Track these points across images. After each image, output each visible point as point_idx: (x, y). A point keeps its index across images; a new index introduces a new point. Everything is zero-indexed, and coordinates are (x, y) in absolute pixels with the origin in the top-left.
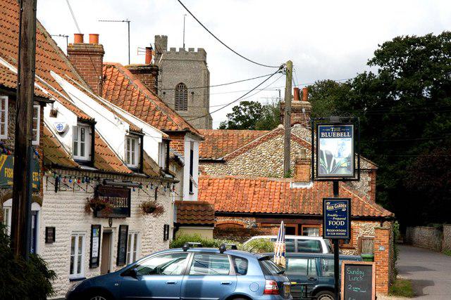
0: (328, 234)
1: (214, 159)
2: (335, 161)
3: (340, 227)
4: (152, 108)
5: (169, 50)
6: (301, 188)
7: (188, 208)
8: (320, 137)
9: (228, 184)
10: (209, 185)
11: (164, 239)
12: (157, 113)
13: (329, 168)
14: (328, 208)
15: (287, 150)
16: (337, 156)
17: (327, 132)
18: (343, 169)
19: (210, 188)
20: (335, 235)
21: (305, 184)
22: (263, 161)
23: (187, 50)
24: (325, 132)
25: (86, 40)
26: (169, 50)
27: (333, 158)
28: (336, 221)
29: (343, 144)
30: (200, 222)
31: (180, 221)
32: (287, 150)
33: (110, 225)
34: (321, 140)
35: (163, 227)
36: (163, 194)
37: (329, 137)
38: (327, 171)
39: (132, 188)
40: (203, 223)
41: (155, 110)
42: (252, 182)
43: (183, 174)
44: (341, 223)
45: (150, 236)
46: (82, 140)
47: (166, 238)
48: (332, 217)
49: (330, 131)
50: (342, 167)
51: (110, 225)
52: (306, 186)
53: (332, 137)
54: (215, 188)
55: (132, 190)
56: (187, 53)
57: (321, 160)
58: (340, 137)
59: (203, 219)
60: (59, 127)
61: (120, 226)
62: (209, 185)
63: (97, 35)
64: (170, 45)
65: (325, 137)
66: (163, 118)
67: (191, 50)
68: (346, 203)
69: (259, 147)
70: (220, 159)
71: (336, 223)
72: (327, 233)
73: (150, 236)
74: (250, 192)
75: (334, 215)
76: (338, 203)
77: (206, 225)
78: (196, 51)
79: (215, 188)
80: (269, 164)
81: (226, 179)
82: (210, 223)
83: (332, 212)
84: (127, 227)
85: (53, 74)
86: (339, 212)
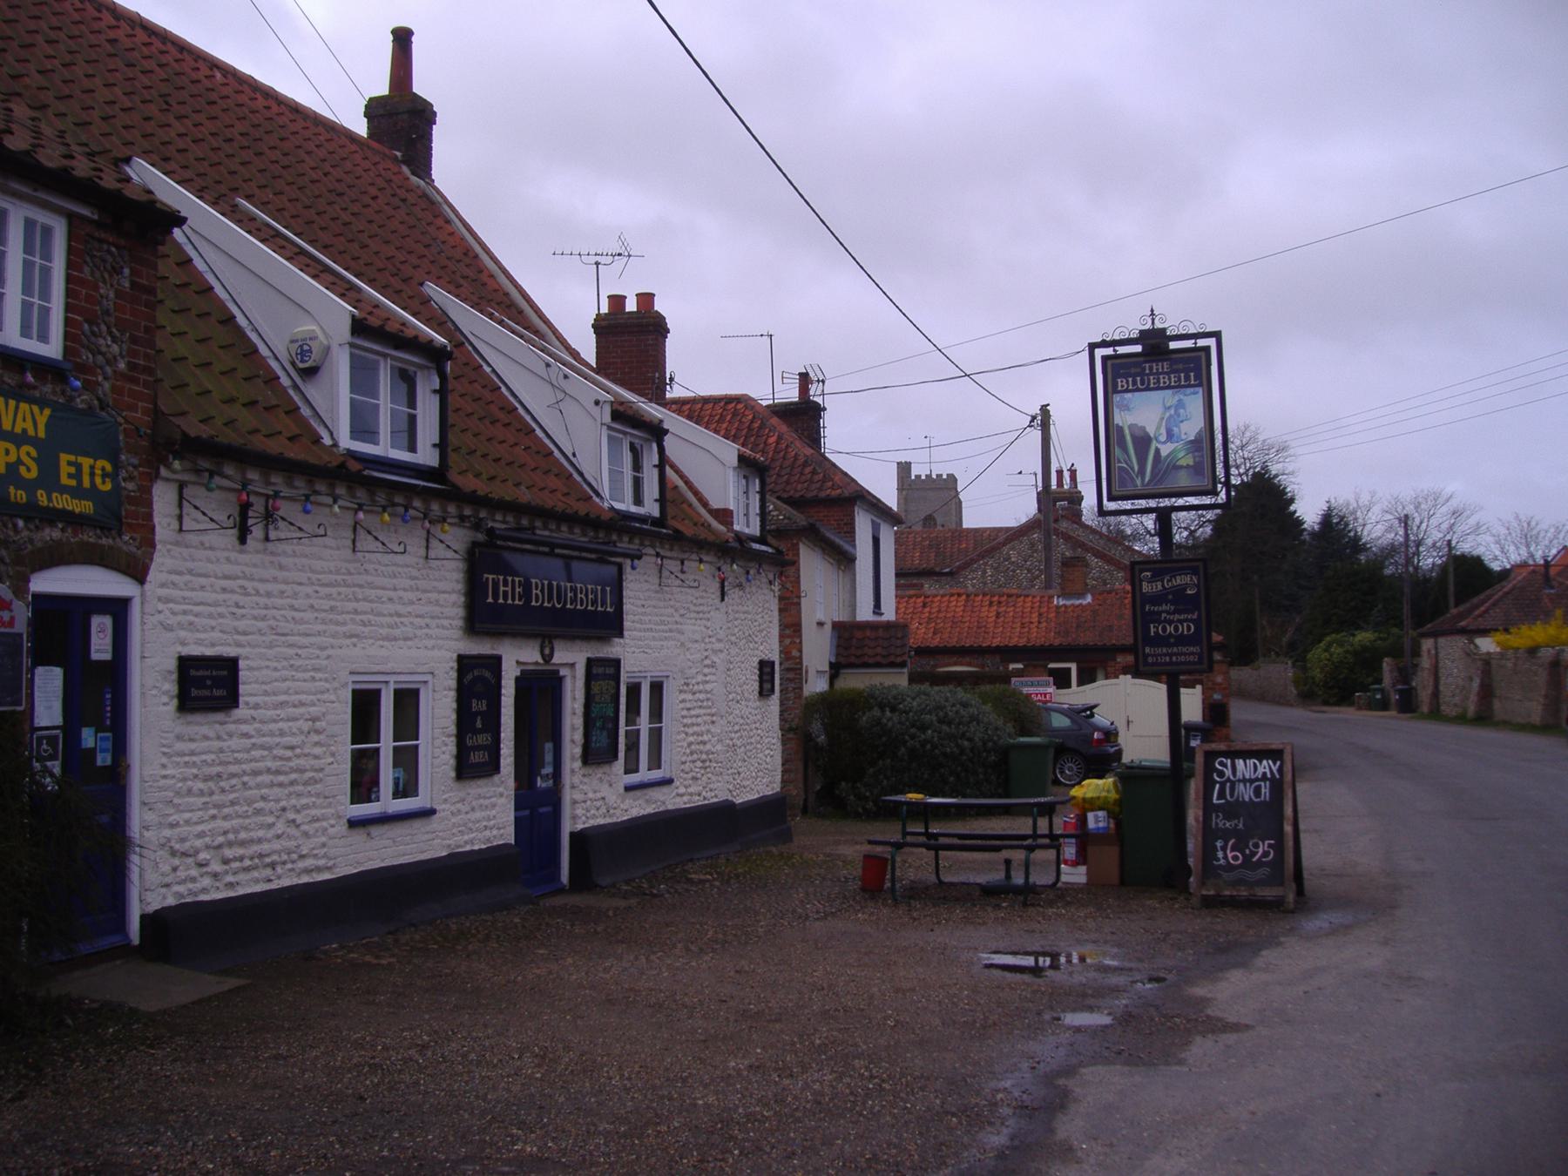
0: (1150, 660)
1: (937, 569)
2: (1157, 451)
3: (1182, 640)
4: (799, 462)
5: (913, 478)
6: (1073, 605)
7: (859, 634)
8: (1116, 391)
9: (954, 603)
10: (924, 606)
11: (761, 694)
12: (808, 470)
13: (1142, 471)
14: (1146, 587)
15: (1048, 548)
16: (1163, 438)
17: (1134, 376)
18: (1183, 473)
19: (927, 610)
20: (1171, 663)
21: (1078, 599)
22: (1014, 571)
23: (934, 477)
24: (1126, 376)
25: (631, 306)
26: (913, 478)
27: (1154, 445)
28: (1170, 622)
29: (1180, 404)
30: (879, 659)
31: (842, 660)
32: (1048, 548)
33: (547, 658)
34: (1117, 398)
35: (756, 664)
36: (740, 586)
37: (1138, 390)
38: (1139, 482)
39: (628, 562)
40: (871, 661)
41: (805, 464)
42: (996, 599)
43: (854, 575)
44: (1183, 629)
45: (708, 687)
46: (637, 467)
47: (765, 692)
48: (1160, 613)
49: (1142, 374)
50: (1181, 467)
51: (547, 658)
52: (1080, 601)
53: (1148, 389)
54: (934, 610)
55: (627, 568)
56: (934, 480)
57: (1117, 452)
58: (1169, 387)
59: (859, 652)
60: (304, 353)
61: (589, 661)
62: (924, 606)
63: (651, 296)
64: (914, 472)
65: (1127, 391)
66: (816, 478)
67: (939, 476)
68: (1195, 571)
69: (1005, 549)
70: (947, 570)
71: (1170, 629)
72: (1146, 656)
73: (708, 687)
74: (991, 615)
75: (1164, 607)
76: (1174, 572)
77: (892, 665)
78: (945, 477)
79: (934, 610)
80: (1023, 575)
81: (952, 595)
82: (899, 660)
83: (1157, 599)
84: (617, 663)
85: (432, 289)
86: (1178, 596)
